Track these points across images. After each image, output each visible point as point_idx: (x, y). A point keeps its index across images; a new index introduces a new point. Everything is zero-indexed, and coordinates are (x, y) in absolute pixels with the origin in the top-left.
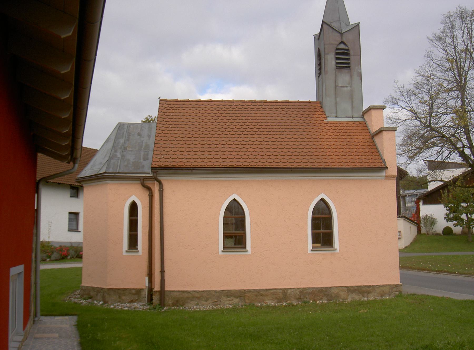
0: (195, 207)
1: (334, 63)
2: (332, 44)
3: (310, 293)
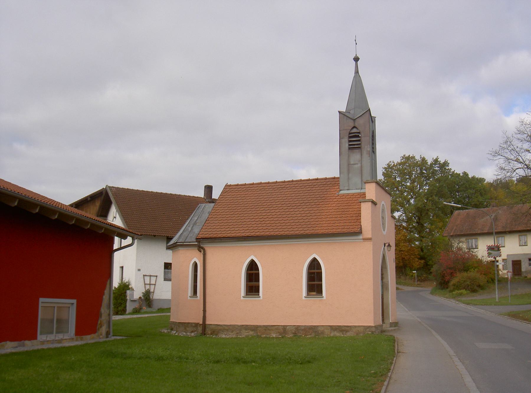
0: (227, 265)
1: (347, 145)
2: (346, 130)
3: (302, 330)
